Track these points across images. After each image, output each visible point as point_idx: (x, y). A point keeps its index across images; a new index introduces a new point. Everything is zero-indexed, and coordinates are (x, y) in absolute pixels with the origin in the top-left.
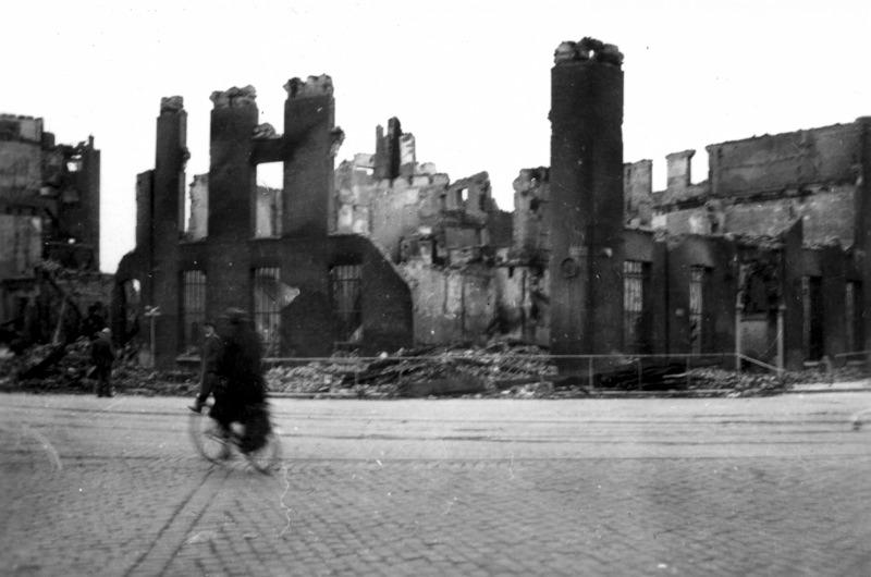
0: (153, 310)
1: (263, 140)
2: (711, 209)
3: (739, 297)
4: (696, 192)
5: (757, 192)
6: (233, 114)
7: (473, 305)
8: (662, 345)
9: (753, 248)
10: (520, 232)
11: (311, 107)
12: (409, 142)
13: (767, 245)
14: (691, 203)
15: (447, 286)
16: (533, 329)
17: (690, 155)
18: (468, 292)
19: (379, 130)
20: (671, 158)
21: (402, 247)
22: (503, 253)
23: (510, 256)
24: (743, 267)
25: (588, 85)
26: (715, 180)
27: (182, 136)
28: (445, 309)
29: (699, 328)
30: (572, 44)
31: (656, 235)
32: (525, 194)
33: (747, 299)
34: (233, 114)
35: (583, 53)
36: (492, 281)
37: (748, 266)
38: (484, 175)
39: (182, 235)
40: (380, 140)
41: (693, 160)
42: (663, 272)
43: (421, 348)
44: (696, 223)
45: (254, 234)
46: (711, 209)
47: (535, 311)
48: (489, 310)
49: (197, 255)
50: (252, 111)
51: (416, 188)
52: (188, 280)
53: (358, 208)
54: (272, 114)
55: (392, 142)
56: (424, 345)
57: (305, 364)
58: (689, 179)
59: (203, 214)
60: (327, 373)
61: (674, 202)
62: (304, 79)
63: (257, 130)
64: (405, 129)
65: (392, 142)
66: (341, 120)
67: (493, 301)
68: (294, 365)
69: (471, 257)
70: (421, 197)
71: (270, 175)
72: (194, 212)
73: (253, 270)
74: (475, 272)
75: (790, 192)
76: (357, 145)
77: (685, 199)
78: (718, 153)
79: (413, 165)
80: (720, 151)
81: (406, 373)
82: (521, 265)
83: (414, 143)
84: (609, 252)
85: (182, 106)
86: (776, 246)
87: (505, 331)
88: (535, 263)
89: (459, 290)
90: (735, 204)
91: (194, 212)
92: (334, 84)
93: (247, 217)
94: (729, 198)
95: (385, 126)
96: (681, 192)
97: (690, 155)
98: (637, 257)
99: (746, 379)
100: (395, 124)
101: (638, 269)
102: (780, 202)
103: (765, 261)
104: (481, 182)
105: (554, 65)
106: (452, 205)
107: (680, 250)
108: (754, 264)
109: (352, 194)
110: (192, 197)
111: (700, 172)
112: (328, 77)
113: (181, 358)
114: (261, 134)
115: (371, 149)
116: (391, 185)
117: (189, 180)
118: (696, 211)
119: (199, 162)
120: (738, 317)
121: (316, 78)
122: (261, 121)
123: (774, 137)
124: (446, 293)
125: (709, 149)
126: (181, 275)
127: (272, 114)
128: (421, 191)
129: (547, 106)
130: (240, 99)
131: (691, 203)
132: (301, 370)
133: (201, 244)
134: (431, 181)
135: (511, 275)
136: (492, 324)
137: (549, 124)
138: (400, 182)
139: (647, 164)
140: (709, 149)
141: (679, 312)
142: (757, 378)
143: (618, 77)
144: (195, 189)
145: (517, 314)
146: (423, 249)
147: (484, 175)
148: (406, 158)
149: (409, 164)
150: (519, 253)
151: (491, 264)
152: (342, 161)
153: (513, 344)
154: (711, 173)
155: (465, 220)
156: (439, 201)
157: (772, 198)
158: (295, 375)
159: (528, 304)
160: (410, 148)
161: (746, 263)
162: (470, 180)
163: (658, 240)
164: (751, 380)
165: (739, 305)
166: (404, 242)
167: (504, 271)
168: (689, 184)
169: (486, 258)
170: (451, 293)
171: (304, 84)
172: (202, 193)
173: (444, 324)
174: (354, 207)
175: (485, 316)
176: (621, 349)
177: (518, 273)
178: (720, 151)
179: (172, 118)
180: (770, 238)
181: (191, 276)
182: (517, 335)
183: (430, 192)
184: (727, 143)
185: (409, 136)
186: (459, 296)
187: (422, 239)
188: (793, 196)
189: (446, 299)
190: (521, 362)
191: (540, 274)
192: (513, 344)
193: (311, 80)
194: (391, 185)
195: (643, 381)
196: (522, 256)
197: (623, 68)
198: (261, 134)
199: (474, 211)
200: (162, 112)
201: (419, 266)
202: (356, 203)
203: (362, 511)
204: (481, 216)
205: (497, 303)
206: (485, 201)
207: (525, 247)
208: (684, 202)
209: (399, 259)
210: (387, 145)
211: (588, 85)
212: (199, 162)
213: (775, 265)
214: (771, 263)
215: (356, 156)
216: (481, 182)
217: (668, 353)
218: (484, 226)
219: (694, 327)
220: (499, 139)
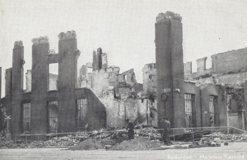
0: (8, 117)
1: (51, 55)
2: (213, 77)
3: (227, 107)
4: (208, 72)
5: (231, 71)
6: (40, 48)
7: (129, 113)
8: (200, 125)
9: (231, 88)
10: (145, 87)
11: (69, 43)
12: (105, 56)
13: (237, 88)
14: (207, 76)
15: (119, 106)
16: (151, 122)
17: (205, 59)
18: (127, 108)
19: (94, 52)
20: (198, 61)
21: (103, 94)
22: (139, 94)
23: (142, 95)
24: (228, 96)
25: (168, 32)
26: (215, 67)
27: (22, 55)
28: (119, 114)
29: (213, 118)
30: (162, 14)
31: (196, 84)
32: (146, 73)
33: (230, 108)
34: (40, 48)
35: (167, 17)
36: (136, 104)
37: (230, 95)
38: (132, 70)
39: (22, 91)
40: (94, 57)
41: (207, 60)
42: (198, 99)
43: (110, 128)
44: (208, 81)
45: (48, 89)
46: (213, 77)
47: (152, 115)
48: (135, 115)
49: (27, 98)
50: (47, 45)
51: (108, 72)
52: (24, 107)
53: (88, 81)
54: (54, 48)
55: (99, 61)
56: (111, 128)
57: (66, 135)
58: (205, 68)
59: (30, 85)
60: (74, 139)
61: (200, 76)
62: (65, 32)
63: (49, 52)
64: (103, 52)
65: (99, 61)
66: (79, 47)
67: (136, 111)
68: (62, 136)
69: (128, 96)
70: (110, 76)
71: (54, 69)
72: (27, 85)
73: (48, 102)
74: (129, 101)
75: (243, 70)
76: (85, 59)
77: (204, 75)
78: (215, 58)
79: (106, 65)
80: (216, 57)
81: (102, 138)
82: (146, 98)
83: (106, 57)
84: (179, 90)
85: (22, 44)
86: (240, 88)
87: (141, 122)
88: (151, 98)
89: (124, 108)
90: (222, 75)
91: (27, 85)
92: (76, 34)
93: (46, 84)
94: (220, 73)
95: (96, 51)
96: (203, 73)
97: (205, 59)
98: (189, 92)
99: (234, 136)
100: (100, 50)
101: (189, 97)
102: (239, 74)
103: (237, 93)
104: (132, 73)
105: (156, 22)
106: (121, 80)
107: (205, 89)
108: (233, 94)
109: (86, 77)
110: (26, 77)
111: (209, 65)
112: (74, 31)
113: (22, 135)
114: (51, 53)
115: (91, 61)
116: (99, 71)
117: (25, 72)
118: (208, 79)
119: (28, 66)
120: (228, 114)
121: (70, 32)
122: (50, 48)
123: (236, 51)
124: (119, 109)
125: (212, 57)
126: (22, 106)
127: (54, 48)
128: (109, 73)
129: (154, 37)
130: (42, 41)
131: (207, 76)
132: (65, 138)
133: (29, 93)
134: (113, 70)
135: (142, 102)
136: (136, 120)
137: (155, 44)
138: (102, 71)
139: (190, 63)
140: (212, 57)
141: (206, 112)
142: (239, 136)
143: (180, 26)
144: (28, 75)
145: (145, 116)
146: (111, 94)
147: (132, 70)
148: (104, 62)
149: (105, 64)
150: (145, 94)
151: (135, 98)
152: (81, 66)
153: (144, 127)
154: (213, 66)
155: (125, 86)
156: (116, 77)
157: (236, 73)
158: (62, 140)
159: (149, 112)
160: (105, 59)
161: (229, 94)
162: (127, 72)
163: (197, 86)
164: (237, 136)
165: (228, 110)
166: (104, 92)
167: (140, 101)
168: (205, 69)
169: (133, 96)
170: (121, 109)
171: (65, 34)
172: (30, 76)
173: (119, 120)
174: (87, 81)
175: (133, 117)
176: (185, 126)
177: (145, 101)
178: (216, 57)
179: (18, 49)
180: (238, 85)
181: (25, 106)
182: (145, 123)
183: (113, 74)
184: (219, 54)
185: (105, 54)
186: (124, 110)
187: (110, 90)
188: (244, 72)
189: (119, 111)
190: (147, 132)
191: (153, 101)
192: (144, 127)
193: (68, 33)
194: (99, 71)
195: (194, 138)
196: (146, 95)
197: (182, 22)
198: (51, 53)
199: (129, 82)
200: (15, 46)
201: (109, 99)
202: (87, 80)
203: (216, 142)
204: (132, 84)
205: (138, 112)
206: (133, 78)
207: (147, 92)
208: (204, 76)
209: (102, 96)
210: (97, 58)
211: (168, 32)
212: (28, 66)
213: (240, 95)
214: (239, 94)
215: (87, 64)
216: (132, 73)
217: (202, 127)
218: (132, 87)
219: (212, 118)
220: (137, 57)
